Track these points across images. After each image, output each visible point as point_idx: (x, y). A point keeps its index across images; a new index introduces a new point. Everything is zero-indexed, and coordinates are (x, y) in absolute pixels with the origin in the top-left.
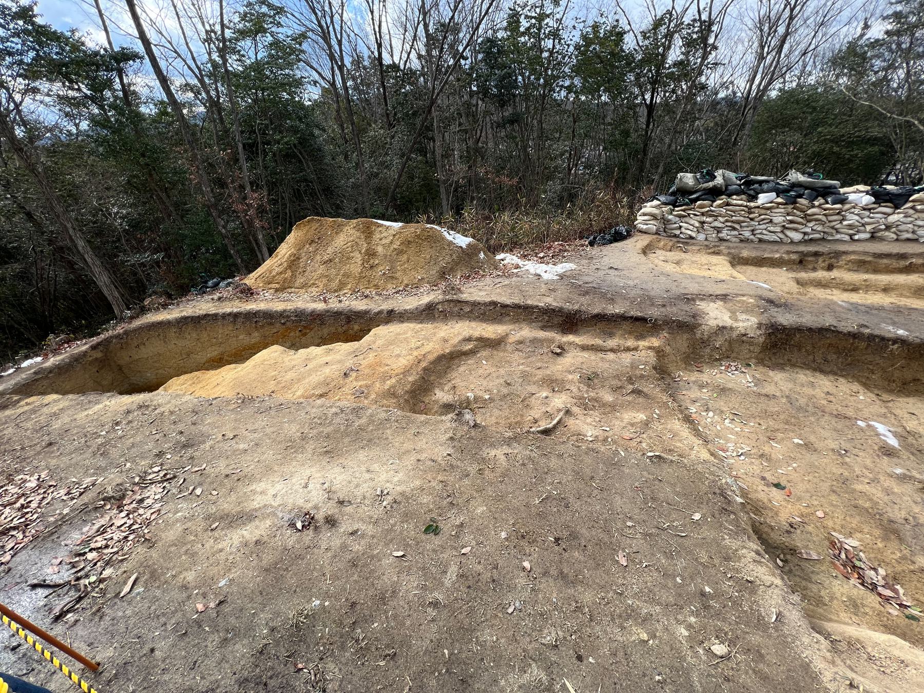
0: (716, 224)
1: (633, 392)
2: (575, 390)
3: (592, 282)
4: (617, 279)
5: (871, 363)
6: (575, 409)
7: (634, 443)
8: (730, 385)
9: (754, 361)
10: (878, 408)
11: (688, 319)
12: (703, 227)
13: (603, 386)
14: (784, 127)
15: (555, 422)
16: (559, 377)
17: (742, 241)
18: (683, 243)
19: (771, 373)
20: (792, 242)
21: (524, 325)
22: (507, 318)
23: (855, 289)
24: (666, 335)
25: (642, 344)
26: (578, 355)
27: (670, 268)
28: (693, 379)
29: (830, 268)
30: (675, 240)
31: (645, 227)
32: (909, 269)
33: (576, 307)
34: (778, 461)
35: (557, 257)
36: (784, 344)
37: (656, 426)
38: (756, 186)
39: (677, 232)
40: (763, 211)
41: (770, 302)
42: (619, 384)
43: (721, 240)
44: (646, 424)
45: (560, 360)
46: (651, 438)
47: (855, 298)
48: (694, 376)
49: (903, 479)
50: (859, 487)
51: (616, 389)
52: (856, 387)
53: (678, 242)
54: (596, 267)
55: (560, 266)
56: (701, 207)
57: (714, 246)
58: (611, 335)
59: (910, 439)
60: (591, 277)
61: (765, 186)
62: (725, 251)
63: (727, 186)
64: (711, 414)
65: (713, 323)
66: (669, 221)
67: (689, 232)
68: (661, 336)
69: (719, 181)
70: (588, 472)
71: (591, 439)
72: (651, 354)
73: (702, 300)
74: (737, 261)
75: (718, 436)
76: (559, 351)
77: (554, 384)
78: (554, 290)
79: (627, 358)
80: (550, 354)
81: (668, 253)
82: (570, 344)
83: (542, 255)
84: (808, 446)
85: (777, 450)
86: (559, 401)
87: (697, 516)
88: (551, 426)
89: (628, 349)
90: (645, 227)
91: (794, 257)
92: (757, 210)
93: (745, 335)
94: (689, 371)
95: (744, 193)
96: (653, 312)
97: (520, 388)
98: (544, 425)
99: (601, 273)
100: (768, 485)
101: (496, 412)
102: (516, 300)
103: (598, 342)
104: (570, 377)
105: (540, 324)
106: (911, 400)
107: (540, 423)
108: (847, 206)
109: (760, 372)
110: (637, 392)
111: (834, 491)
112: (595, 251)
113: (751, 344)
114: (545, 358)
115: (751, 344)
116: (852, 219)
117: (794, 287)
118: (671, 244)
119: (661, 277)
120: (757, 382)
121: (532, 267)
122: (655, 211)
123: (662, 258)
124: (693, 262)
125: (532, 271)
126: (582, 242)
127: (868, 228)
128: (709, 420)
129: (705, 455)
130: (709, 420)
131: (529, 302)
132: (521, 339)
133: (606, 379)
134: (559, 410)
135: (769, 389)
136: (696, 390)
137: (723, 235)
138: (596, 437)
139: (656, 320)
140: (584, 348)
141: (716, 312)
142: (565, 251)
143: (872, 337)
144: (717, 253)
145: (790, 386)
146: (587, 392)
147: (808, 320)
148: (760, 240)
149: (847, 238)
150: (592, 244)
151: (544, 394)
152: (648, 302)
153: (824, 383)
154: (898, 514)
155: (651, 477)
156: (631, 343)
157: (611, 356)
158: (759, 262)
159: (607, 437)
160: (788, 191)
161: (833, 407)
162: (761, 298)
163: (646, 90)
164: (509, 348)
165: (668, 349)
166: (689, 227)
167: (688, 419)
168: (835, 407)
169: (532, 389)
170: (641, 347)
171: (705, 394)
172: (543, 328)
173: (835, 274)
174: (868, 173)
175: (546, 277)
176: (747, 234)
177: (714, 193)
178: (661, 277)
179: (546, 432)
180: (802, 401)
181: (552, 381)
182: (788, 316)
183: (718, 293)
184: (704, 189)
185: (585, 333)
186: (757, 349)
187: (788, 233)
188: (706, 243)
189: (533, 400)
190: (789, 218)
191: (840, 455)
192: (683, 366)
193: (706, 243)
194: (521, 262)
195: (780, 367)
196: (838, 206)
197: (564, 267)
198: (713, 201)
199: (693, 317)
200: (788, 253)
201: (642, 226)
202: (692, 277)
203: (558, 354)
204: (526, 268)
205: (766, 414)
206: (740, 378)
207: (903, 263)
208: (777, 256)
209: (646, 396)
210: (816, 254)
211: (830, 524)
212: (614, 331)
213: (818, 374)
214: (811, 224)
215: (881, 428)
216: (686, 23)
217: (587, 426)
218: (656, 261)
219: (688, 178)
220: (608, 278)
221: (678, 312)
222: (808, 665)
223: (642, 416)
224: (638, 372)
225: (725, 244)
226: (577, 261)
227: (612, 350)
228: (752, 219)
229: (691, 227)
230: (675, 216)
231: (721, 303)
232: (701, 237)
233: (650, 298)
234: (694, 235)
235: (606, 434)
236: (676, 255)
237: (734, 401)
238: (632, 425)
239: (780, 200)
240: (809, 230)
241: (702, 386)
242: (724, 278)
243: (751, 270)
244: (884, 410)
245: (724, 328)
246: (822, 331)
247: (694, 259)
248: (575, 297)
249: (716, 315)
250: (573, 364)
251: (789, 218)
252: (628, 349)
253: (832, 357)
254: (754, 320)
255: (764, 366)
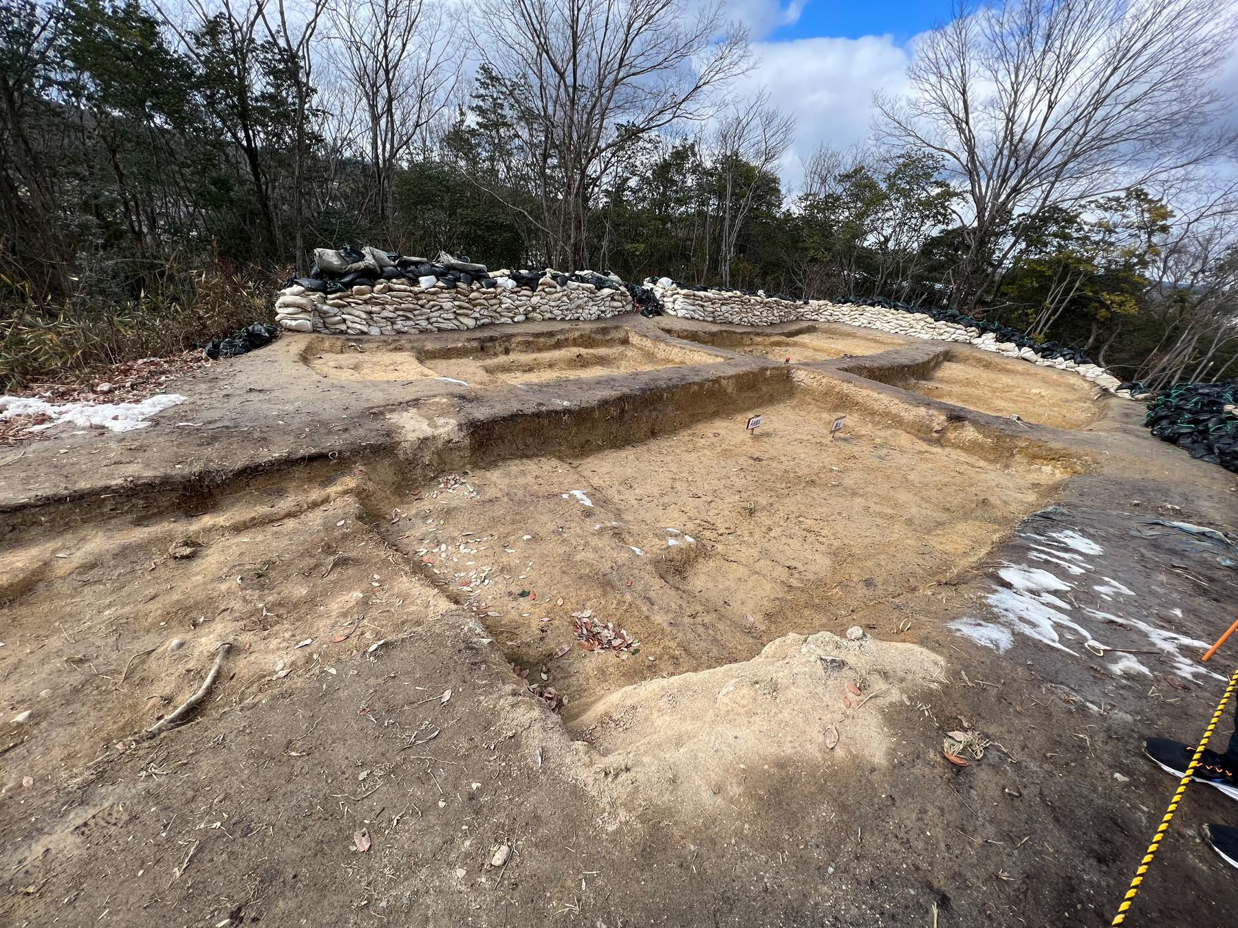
0: (385, 314)
1: (336, 565)
2: (237, 605)
3: (221, 419)
4: (266, 406)
5: (556, 437)
6: (246, 638)
7: (353, 641)
8: (454, 504)
9: (468, 466)
10: (573, 477)
11: (382, 440)
12: (372, 318)
13: (287, 578)
14: (427, 204)
15: (208, 680)
16: (201, 596)
17: (421, 332)
18: (355, 340)
19: (488, 474)
20: (468, 329)
21: (88, 531)
22: (34, 531)
23: (530, 369)
24: (361, 468)
25: (332, 490)
26: (227, 544)
27: (346, 376)
28: (414, 512)
29: (507, 352)
30: (343, 337)
31: (294, 323)
32: (558, 345)
33: (197, 468)
34: (517, 566)
35: (140, 388)
36: (494, 438)
37: (380, 599)
38: (412, 267)
39: (343, 327)
40: (430, 297)
41: (462, 397)
42: (313, 561)
43: (399, 332)
44: (365, 603)
45: (196, 566)
46: (375, 619)
47: (533, 378)
48: (414, 509)
49: (601, 532)
50: (578, 557)
51: (308, 574)
52: (554, 462)
53: (348, 340)
54: (225, 392)
55: (149, 401)
56: (362, 293)
57: (394, 341)
58: (281, 493)
59: (598, 495)
60: (218, 411)
61: (422, 268)
62: (408, 346)
63: (381, 267)
64: (443, 547)
65: (412, 437)
66: (325, 313)
67: (359, 327)
68: (356, 471)
69: (369, 260)
70: (278, 738)
71: (283, 673)
72: (349, 499)
73: (392, 411)
74: (424, 356)
75: (457, 571)
76: (188, 551)
77: (190, 615)
78: (142, 449)
79: (315, 519)
80: (172, 563)
81: (340, 357)
82: (208, 531)
83: (105, 387)
84: (536, 538)
85: (513, 555)
86: (208, 641)
87: (447, 695)
88: (200, 693)
89: (315, 505)
90: (294, 323)
91: (475, 344)
92: (423, 296)
93: (450, 441)
94: (407, 503)
95: (404, 277)
96: (333, 443)
97: (114, 655)
98: (185, 699)
99: (235, 402)
100: (515, 599)
101: (60, 735)
102: (45, 487)
103: (262, 510)
104: (223, 587)
105: (129, 517)
106: (589, 460)
107: (179, 699)
108: (499, 290)
109: (476, 477)
110: (342, 562)
111: (564, 572)
112: (221, 367)
113: (459, 449)
114: (163, 573)
115: (459, 449)
116: (507, 302)
117: (482, 375)
118: (339, 343)
119: (333, 391)
120: (479, 489)
121: (81, 413)
122: (299, 300)
123: (332, 364)
124: (375, 364)
125: (81, 421)
126: (196, 354)
127: (521, 310)
128: (443, 555)
129: (444, 605)
130: (443, 555)
131: (83, 485)
132: (91, 558)
133: (289, 564)
134: (212, 656)
135: (491, 492)
136: (421, 524)
137: (399, 325)
138: (293, 663)
139: (340, 453)
140: (238, 529)
141: (413, 423)
142: (163, 373)
143: (549, 413)
144: (399, 349)
145: (507, 481)
146: (261, 598)
147: (500, 410)
148: (439, 329)
149: (510, 321)
150: (214, 355)
151: (175, 641)
152: (322, 431)
153: (531, 466)
154: (606, 566)
155: (380, 681)
156: (315, 494)
157: (291, 524)
158: (447, 354)
159: (311, 654)
160: (446, 274)
161: (543, 489)
162: (452, 395)
163: (235, 126)
164: (62, 588)
165: (370, 486)
166: (355, 318)
167: (420, 569)
168: (546, 489)
169: (147, 642)
170: (333, 495)
171: (431, 526)
172: (138, 523)
173: (513, 356)
174: (510, 256)
175: (117, 427)
176: (424, 323)
177: (370, 276)
178: (333, 391)
179: (193, 712)
180: (878, 441)
181: (188, 610)
182: (482, 409)
183: (408, 398)
184: (356, 271)
185: (233, 504)
186: (468, 454)
187: (461, 319)
188: (383, 338)
189: (152, 663)
190: (457, 303)
191: (560, 534)
192: (398, 500)
193: (383, 338)
194: (50, 410)
195: (492, 465)
196: (492, 290)
197: (154, 404)
198: (373, 286)
199: (388, 435)
200: (469, 340)
201: (289, 322)
202: (374, 384)
203: (188, 557)
204: (66, 418)
205: (495, 521)
206: (458, 492)
207: (553, 341)
208: (460, 345)
209: (356, 562)
210: (492, 339)
211: (569, 606)
212: (283, 484)
213: (525, 461)
214: (477, 309)
215: (578, 494)
216: (259, 42)
217: (274, 656)
218: (326, 369)
219: (330, 256)
220: (250, 407)
221: (365, 434)
222: (575, 786)
223: (357, 595)
224: (336, 533)
225: (405, 337)
226: (186, 387)
227: (290, 515)
228: (422, 306)
229: (357, 320)
230: (332, 305)
231: (415, 410)
232: (374, 331)
233: (325, 424)
234: (365, 329)
235: (309, 650)
236: (349, 358)
237: (462, 519)
238: (345, 615)
239: (440, 284)
240: (478, 315)
241: (425, 518)
242: (411, 378)
243: (441, 364)
244: (576, 476)
245: (426, 439)
246: (514, 417)
247: (375, 360)
248: (193, 450)
249: (412, 426)
250: (225, 563)
251: (457, 303)
252: (315, 505)
253: (530, 440)
254: (453, 422)
255: (480, 468)
